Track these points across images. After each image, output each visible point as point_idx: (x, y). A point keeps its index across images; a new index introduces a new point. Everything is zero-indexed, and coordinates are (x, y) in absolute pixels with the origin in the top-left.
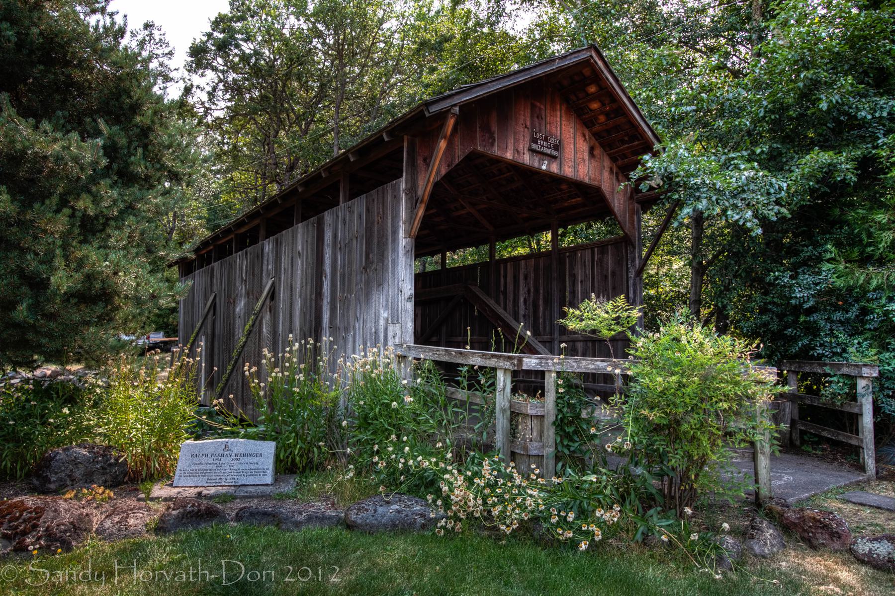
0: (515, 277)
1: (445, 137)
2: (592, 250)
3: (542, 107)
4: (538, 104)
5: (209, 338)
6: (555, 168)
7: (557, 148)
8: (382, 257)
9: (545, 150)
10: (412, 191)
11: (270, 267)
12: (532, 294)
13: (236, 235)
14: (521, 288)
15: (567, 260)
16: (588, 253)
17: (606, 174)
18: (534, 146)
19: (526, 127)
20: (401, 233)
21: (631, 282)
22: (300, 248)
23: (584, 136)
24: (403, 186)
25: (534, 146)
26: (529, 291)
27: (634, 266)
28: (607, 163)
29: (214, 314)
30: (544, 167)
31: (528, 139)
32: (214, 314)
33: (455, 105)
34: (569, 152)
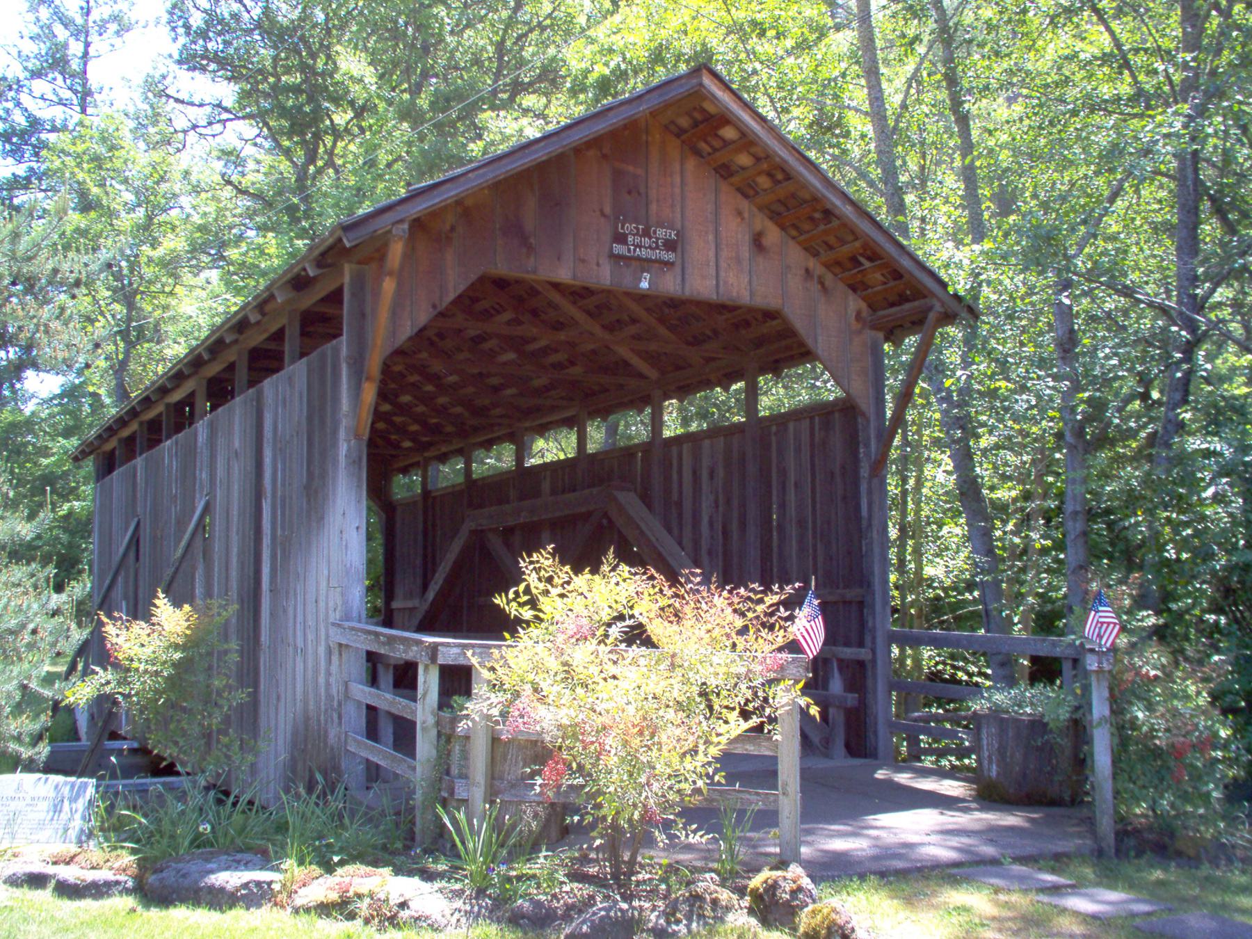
0: (694, 472)
1: (390, 274)
2: (812, 418)
3: (640, 172)
4: (631, 168)
5: (131, 603)
6: (670, 285)
7: (670, 245)
8: (323, 476)
9: (643, 253)
10: (358, 363)
11: (204, 476)
12: (721, 509)
13: (168, 405)
14: (704, 498)
15: (774, 439)
16: (806, 424)
17: (795, 282)
18: (618, 249)
19: (603, 214)
20: (342, 434)
21: (864, 487)
22: (237, 444)
23: (739, 213)
24: (344, 351)
25: (618, 249)
26: (716, 502)
27: (868, 454)
28: (796, 255)
29: (137, 559)
30: (644, 285)
31: (607, 237)
32: (137, 559)
33: (401, 221)
34: (700, 249)
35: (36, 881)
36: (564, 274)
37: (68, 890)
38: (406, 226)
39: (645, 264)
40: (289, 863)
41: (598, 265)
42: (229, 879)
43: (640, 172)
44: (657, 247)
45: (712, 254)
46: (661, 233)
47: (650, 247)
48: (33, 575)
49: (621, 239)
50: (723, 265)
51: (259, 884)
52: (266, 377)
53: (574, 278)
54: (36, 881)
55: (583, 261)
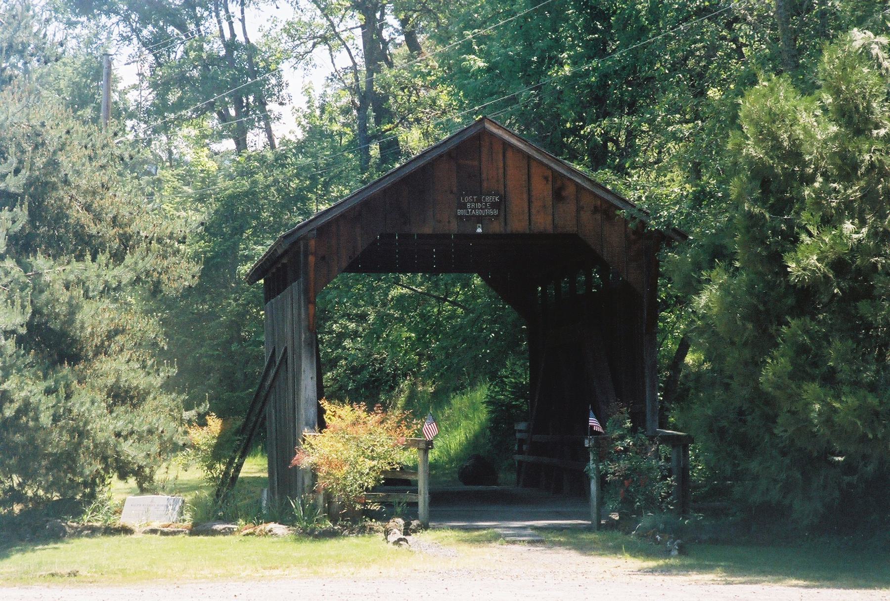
18: (460, 212)
25: (460, 212)
30: (479, 230)
35: (154, 531)
36: (427, 230)
37: (164, 533)
38: (315, 232)
39: (479, 219)
40: (241, 522)
41: (449, 222)
42: (219, 527)
43: (476, 163)
44: (486, 207)
45: (526, 205)
46: (488, 199)
47: (481, 208)
48: (174, 400)
49: (463, 206)
50: (533, 211)
51: (229, 529)
52: (222, 430)
53: (555, 226)
54: (154, 531)
55: (440, 222)
